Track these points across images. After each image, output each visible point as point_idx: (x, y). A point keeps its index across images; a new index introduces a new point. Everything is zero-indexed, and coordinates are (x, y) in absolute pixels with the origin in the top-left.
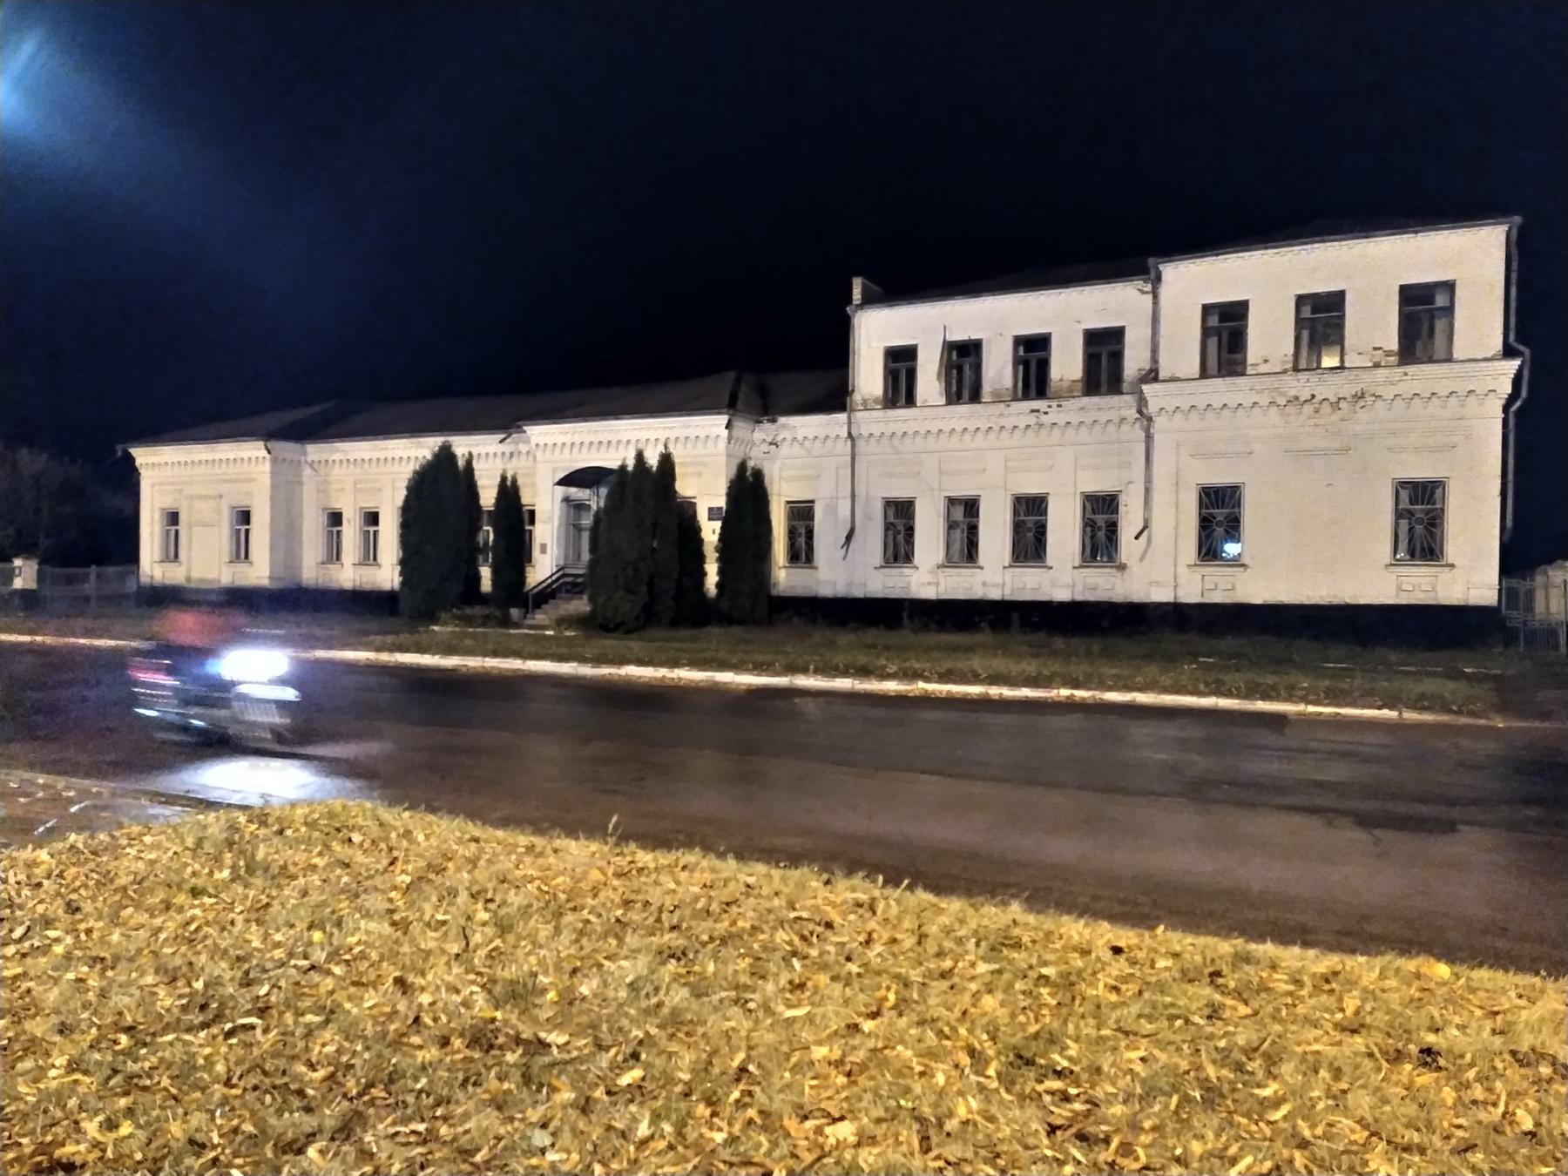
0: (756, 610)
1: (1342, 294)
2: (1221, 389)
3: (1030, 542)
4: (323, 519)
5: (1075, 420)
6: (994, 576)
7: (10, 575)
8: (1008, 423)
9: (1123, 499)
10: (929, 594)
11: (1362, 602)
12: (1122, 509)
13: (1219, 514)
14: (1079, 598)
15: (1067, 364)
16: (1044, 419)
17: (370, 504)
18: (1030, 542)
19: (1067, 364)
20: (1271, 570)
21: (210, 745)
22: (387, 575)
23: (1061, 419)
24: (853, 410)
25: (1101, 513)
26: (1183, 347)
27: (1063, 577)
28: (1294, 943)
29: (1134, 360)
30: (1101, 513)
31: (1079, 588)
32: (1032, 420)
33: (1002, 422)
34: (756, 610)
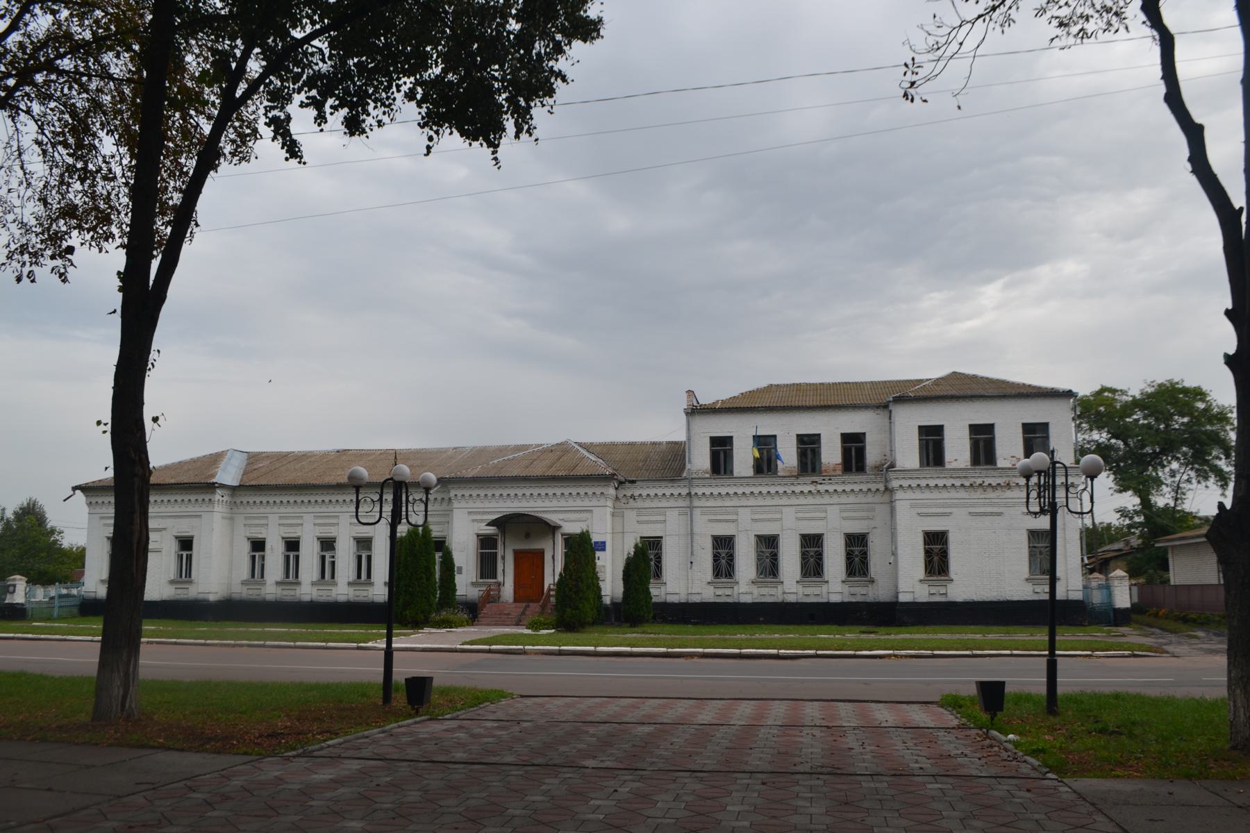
0: (639, 608)
1: (992, 425)
2: (933, 477)
3: (812, 566)
4: (246, 547)
5: (840, 488)
6: (791, 585)
7: (11, 590)
8: (798, 489)
9: (871, 538)
10: (747, 599)
11: (1015, 599)
12: (870, 544)
13: (936, 552)
14: (846, 600)
15: (831, 454)
16: (820, 487)
17: (292, 533)
18: (812, 566)
19: (831, 454)
20: (968, 582)
21: (1185, 620)
22: (378, 591)
23: (831, 488)
24: (690, 481)
25: (857, 546)
26: (908, 454)
27: (835, 586)
28: (1142, 403)
29: (872, 455)
30: (857, 546)
31: (800, 596)
32: (812, 488)
33: (793, 488)
34: (639, 608)
